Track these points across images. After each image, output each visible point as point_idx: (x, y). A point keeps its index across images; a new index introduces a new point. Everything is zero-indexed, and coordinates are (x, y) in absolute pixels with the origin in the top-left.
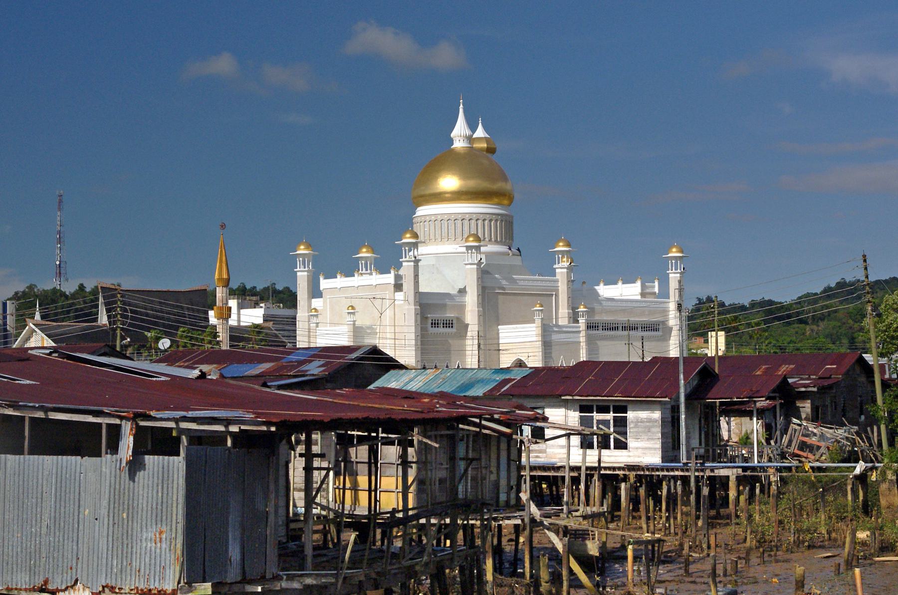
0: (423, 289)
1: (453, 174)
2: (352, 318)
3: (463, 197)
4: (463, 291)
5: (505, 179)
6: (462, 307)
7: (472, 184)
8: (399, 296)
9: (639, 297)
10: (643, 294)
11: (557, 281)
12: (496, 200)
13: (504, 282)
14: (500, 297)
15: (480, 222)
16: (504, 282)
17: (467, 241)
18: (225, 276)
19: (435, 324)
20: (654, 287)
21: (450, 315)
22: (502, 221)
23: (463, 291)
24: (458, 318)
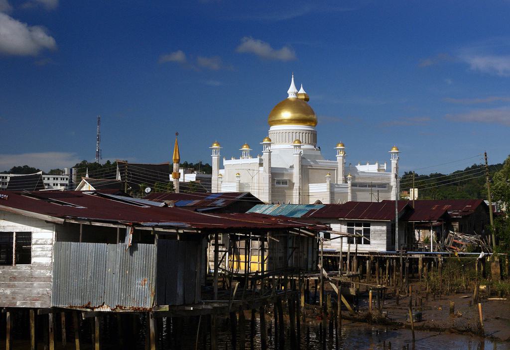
0: (272, 166)
1: (281, 109)
2: (238, 179)
3: (293, 122)
4: (292, 167)
5: (313, 113)
6: (291, 175)
7: (297, 115)
8: (261, 169)
9: (377, 171)
10: (379, 170)
11: (338, 163)
12: (308, 124)
13: (312, 163)
14: (310, 170)
15: (298, 134)
16: (312, 163)
17: (294, 143)
18: (178, 158)
19: (278, 183)
20: (384, 167)
21: (286, 178)
22: (311, 134)
23: (292, 167)
24: (289, 180)
